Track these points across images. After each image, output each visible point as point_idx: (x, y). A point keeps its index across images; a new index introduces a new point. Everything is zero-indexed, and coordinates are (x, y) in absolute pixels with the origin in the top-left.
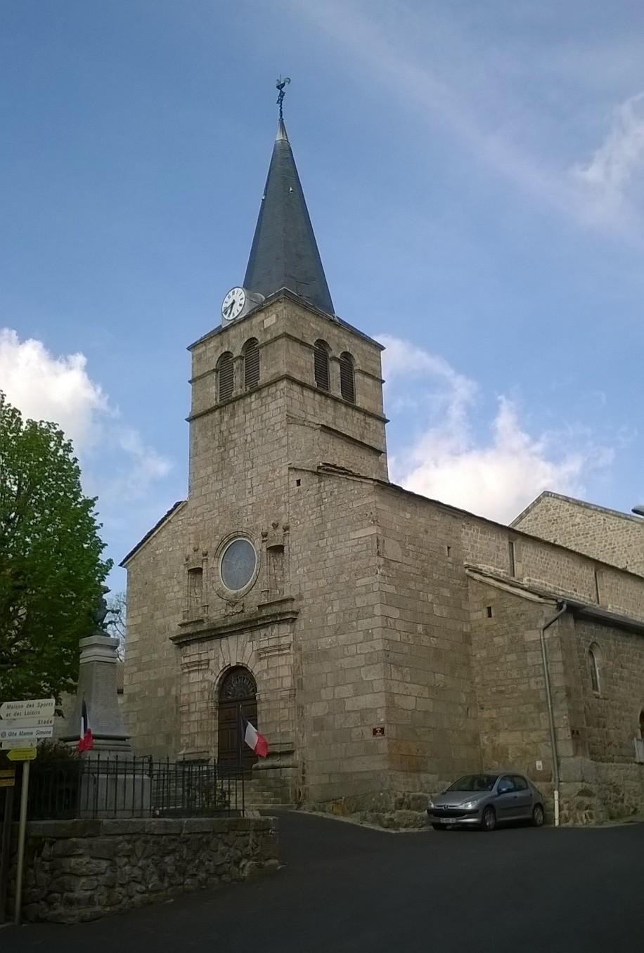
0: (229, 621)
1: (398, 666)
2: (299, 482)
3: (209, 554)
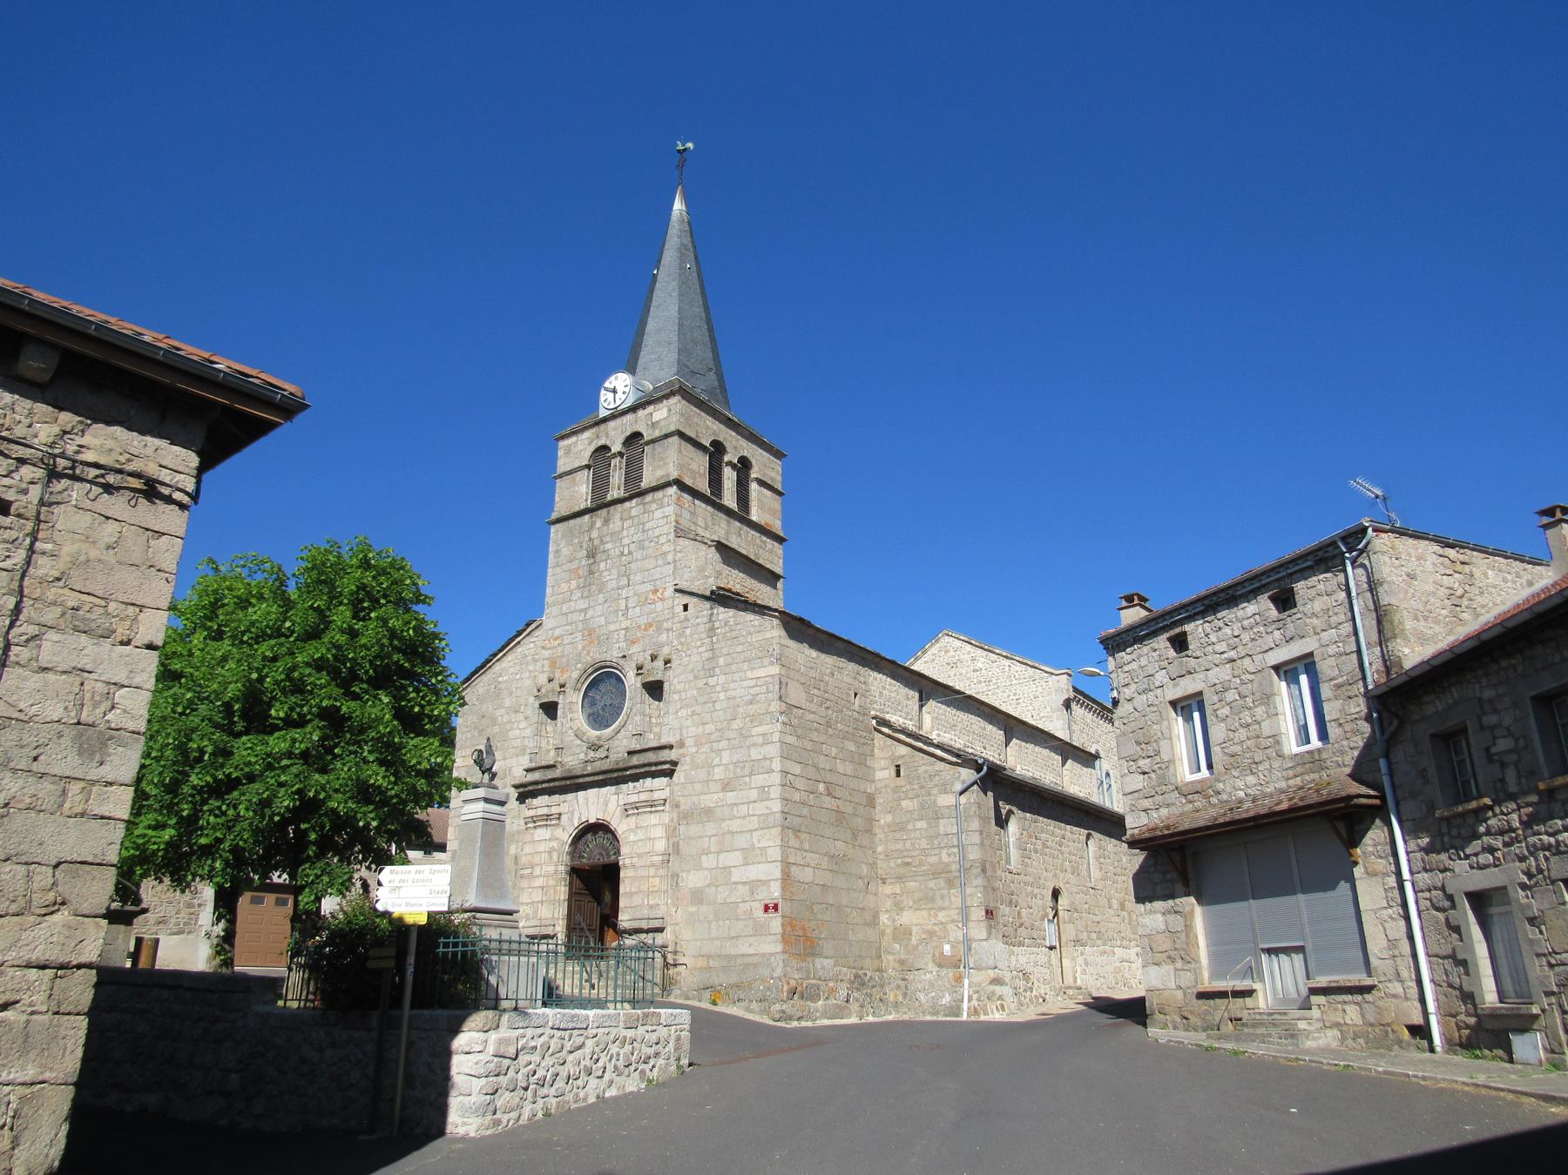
0: (589, 768)
1: (797, 831)
2: (686, 608)
3: (568, 685)
